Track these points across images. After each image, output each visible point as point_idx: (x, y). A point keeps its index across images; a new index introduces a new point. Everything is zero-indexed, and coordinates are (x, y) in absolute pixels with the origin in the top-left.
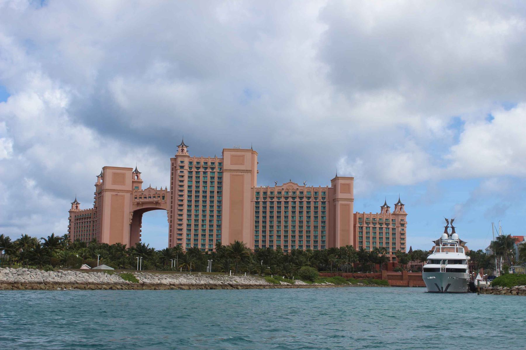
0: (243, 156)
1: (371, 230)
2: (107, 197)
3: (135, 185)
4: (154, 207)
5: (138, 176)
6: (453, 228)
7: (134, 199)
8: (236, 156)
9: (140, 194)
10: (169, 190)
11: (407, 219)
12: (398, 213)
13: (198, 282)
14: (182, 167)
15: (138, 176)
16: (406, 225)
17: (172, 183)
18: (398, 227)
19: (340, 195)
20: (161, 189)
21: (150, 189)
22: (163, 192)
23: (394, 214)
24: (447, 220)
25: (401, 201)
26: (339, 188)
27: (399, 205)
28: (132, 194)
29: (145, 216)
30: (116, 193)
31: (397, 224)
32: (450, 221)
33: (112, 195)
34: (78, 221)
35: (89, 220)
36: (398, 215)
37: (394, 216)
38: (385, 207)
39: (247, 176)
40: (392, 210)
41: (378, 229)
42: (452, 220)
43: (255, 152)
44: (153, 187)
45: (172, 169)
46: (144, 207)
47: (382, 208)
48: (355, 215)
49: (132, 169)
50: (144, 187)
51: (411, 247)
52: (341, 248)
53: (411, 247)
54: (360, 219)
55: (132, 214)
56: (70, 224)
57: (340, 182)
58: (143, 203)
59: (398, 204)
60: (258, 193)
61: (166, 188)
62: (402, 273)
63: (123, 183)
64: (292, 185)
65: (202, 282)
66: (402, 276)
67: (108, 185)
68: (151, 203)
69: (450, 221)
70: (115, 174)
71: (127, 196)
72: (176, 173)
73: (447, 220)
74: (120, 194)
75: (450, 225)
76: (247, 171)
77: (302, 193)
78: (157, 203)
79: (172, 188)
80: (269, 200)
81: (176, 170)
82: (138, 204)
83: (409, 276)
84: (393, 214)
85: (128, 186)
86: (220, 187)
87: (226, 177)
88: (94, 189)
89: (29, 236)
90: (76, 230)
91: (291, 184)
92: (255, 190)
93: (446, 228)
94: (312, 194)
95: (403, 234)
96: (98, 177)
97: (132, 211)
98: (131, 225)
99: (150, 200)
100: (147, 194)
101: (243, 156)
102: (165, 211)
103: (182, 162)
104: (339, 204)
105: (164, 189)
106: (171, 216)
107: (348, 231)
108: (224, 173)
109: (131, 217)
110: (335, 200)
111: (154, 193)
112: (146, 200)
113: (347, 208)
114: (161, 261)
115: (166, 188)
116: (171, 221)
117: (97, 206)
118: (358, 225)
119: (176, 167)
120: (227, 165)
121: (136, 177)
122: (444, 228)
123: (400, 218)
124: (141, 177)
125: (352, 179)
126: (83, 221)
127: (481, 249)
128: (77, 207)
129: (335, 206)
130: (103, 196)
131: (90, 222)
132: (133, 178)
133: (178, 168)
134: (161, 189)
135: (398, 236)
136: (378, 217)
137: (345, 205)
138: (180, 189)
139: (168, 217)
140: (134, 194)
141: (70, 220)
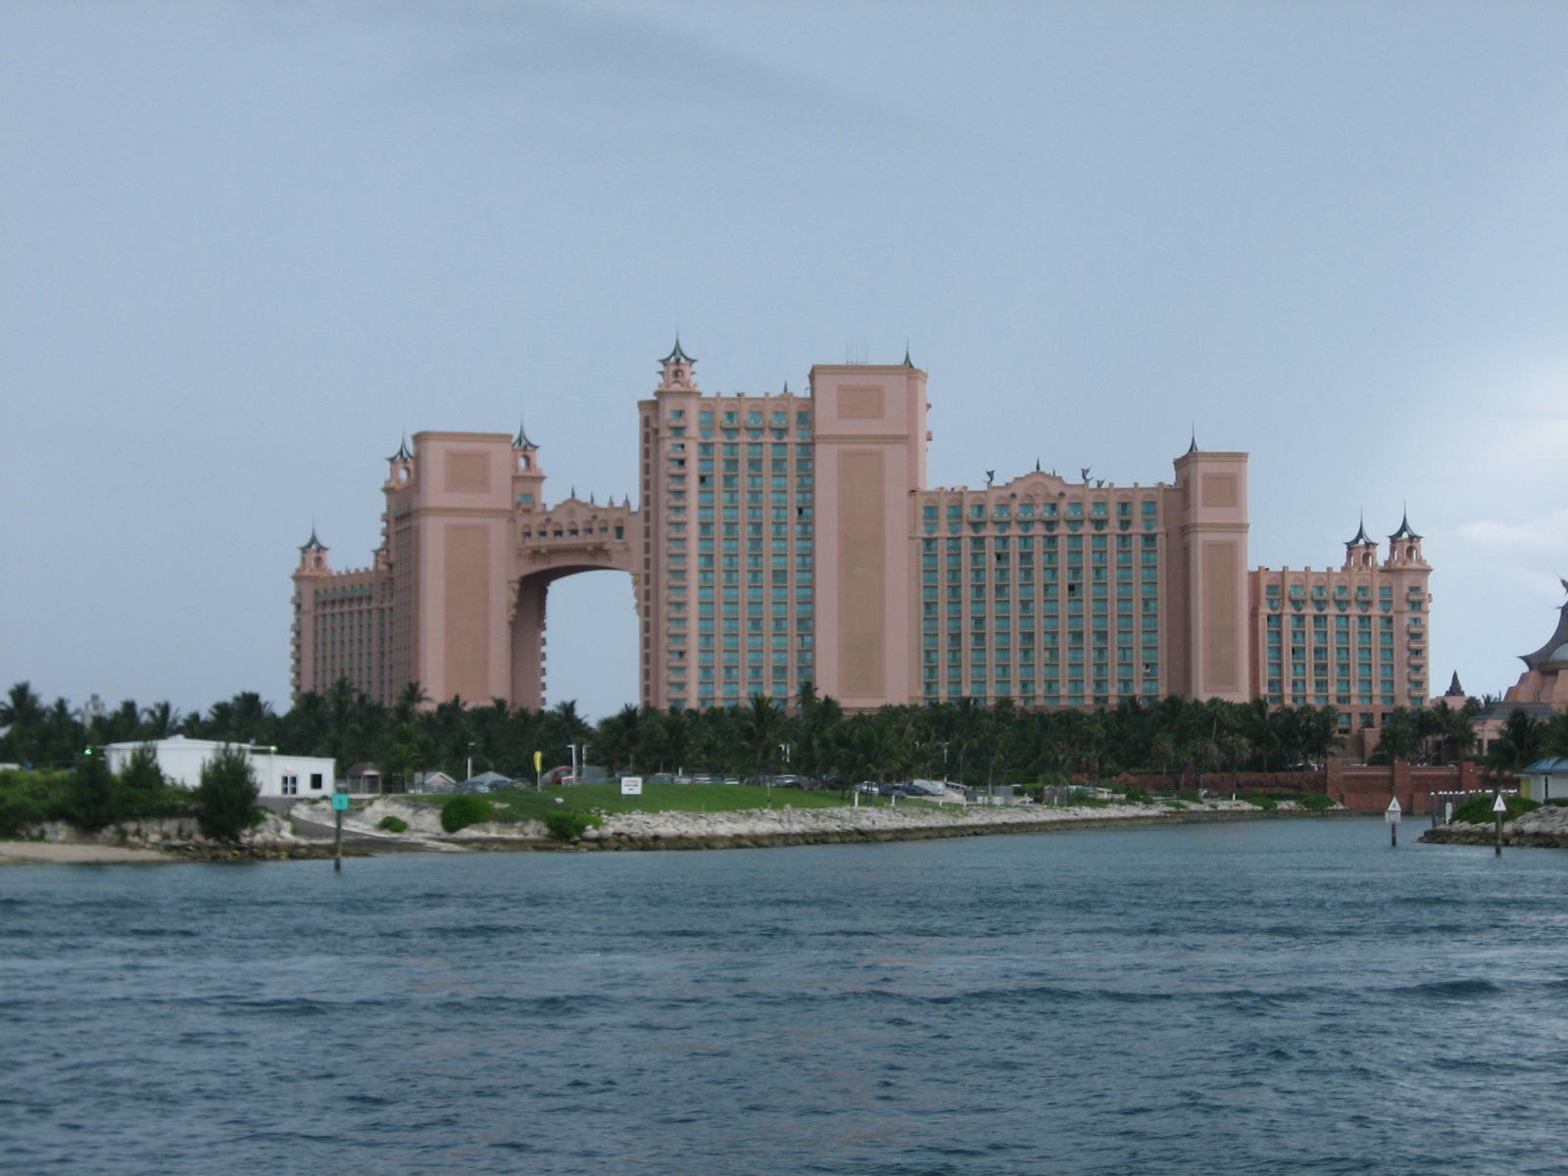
1: (1354, 625)
2: (434, 535)
3: (520, 487)
4: (593, 559)
5: (528, 459)
7: (520, 538)
9: (542, 519)
10: (635, 506)
11: (1433, 585)
12: (1399, 565)
13: (787, 826)
14: (679, 430)
15: (528, 459)
16: (1431, 606)
17: (646, 485)
18: (1402, 612)
19: (1204, 514)
20: (611, 503)
22: (618, 515)
23: (1388, 569)
25: (1410, 523)
26: (1198, 489)
27: (1405, 540)
28: (512, 520)
29: (557, 589)
31: (1399, 602)
34: (328, 610)
35: (364, 606)
36: (1400, 571)
37: (1386, 576)
38: (1359, 548)
39: (894, 454)
40: (1382, 554)
41: (1309, 620)
43: (918, 371)
44: (583, 496)
45: (646, 438)
47: (1351, 546)
48: (1255, 577)
49: (510, 437)
50: (551, 496)
51: (1455, 676)
52: (828, 700)
53: (1455, 676)
54: (1273, 588)
55: (517, 586)
56: (298, 620)
57: (1203, 468)
58: (553, 552)
60: (931, 512)
61: (627, 502)
62: (1461, 770)
63: (482, 484)
64: (1046, 481)
65: (797, 828)
66: (1392, 778)
67: (435, 492)
68: (581, 550)
70: (454, 457)
71: (498, 529)
72: (657, 451)
76: (896, 439)
77: (1078, 505)
78: (599, 550)
79: (646, 500)
80: (967, 532)
81: (657, 441)
82: (536, 554)
83: (1414, 778)
84: (1382, 571)
85: (500, 495)
86: (807, 489)
87: (826, 459)
88: (381, 503)
91: (1040, 479)
92: (921, 501)
94: (1113, 510)
95: (1416, 637)
96: (392, 460)
97: (516, 576)
98: (515, 625)
99: (574, 541)
103: (681, 413)
104: (1200, 540)
105: (619, 503)
106: (647, 593)
107: (1231, 631)
108: (819, 448)
109: (514, 599)
110: (1186, 530)
111: (588, 516)
112: (559, 541)
113: (1229, 554)
115: (627, 502)
116: (647, 608)
117: (392, 558)
118: (1265, 610)
119: (657, 431)
120: (827, 419)
121: (522, 463)
123: (1407, 581)
124: (541, 460)
125: (1240, 457)
126: (346, 608)
128: (319, 560)
129: (1186, 550)
130: (418, 530)
131: (369, 611)
132: (516, 468)
133: (665, 433)
134: (611, 503)
135: (1400, 641)
136: (1334, 581)
137: (1221, 545)
138: (674, 503)
139: (637, 595)
140: (523, 520)
141: (299, 607)
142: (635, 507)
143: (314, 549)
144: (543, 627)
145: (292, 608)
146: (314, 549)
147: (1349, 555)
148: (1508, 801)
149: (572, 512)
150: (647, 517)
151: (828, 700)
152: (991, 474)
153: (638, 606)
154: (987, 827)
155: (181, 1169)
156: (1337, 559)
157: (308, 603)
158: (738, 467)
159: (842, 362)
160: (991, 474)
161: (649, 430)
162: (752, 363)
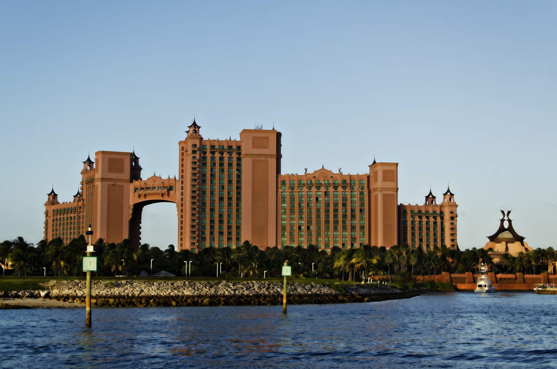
0: (267, 138)
6: (510, 221)
8: (264, 148)
21: (154, 178)
24: (503, 212)
27: (449, 194)
29: (146, 210)
30: (113, 183)
32: (506, 213)
33: (109, 186)
38: (430, 198)
42: (509, 212)
46: (148, 199)
47: (427, 198)
59: (446, 193)
63: (121, 171)
69: (506, 213)
73: (503, 212)
74: (118, 183)
75: (506, 218)
87: (246, 163)
89: (542, 248)
90: (55, 228)
93: (502, 221)
96: (84, 162)
100: (150, 185)
101: (267, 138)
102: (175, 205)
114: (167, 264)
122: (500, 222)
127: (147, 243)
139: (178, 210)
142: (177, 178)
143: (53, 195)
144: (141, 223)
145: (45, 216)
146: (53, 195)
147: (426, 201)
148: (276, 273)
149: (154, 181)
150: (182, 183)
151: (401, 204)
152: (306, 170)
153: (178, 214)
154: (327, 302)
155: (82, 367)
156: (421, 202)
157: (50, 214)
158: (216, 169)
159: (253, 128)
160: (306, 170)
161: (184, 151)
162: (220, 129)
